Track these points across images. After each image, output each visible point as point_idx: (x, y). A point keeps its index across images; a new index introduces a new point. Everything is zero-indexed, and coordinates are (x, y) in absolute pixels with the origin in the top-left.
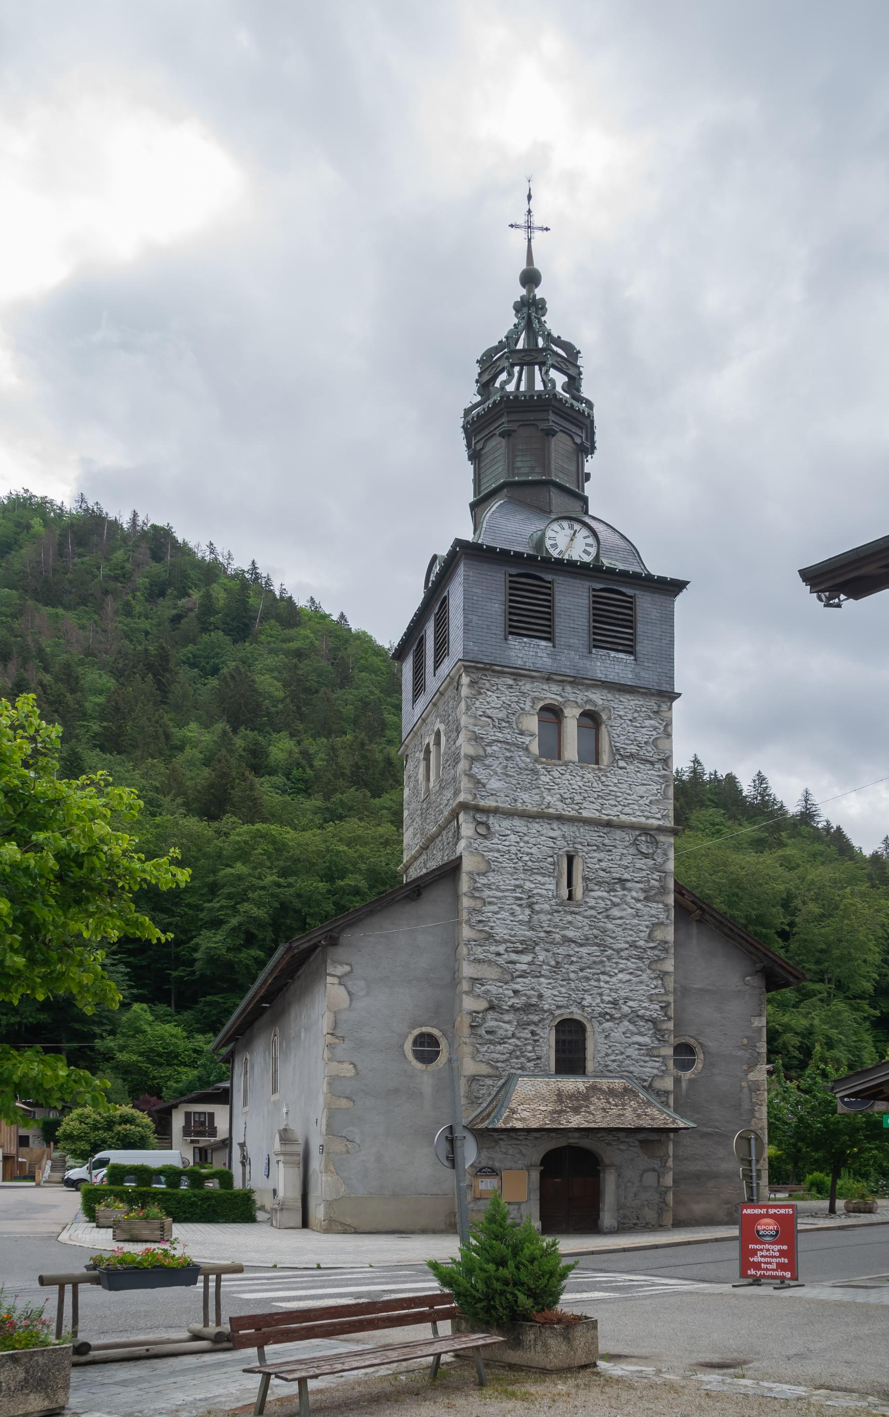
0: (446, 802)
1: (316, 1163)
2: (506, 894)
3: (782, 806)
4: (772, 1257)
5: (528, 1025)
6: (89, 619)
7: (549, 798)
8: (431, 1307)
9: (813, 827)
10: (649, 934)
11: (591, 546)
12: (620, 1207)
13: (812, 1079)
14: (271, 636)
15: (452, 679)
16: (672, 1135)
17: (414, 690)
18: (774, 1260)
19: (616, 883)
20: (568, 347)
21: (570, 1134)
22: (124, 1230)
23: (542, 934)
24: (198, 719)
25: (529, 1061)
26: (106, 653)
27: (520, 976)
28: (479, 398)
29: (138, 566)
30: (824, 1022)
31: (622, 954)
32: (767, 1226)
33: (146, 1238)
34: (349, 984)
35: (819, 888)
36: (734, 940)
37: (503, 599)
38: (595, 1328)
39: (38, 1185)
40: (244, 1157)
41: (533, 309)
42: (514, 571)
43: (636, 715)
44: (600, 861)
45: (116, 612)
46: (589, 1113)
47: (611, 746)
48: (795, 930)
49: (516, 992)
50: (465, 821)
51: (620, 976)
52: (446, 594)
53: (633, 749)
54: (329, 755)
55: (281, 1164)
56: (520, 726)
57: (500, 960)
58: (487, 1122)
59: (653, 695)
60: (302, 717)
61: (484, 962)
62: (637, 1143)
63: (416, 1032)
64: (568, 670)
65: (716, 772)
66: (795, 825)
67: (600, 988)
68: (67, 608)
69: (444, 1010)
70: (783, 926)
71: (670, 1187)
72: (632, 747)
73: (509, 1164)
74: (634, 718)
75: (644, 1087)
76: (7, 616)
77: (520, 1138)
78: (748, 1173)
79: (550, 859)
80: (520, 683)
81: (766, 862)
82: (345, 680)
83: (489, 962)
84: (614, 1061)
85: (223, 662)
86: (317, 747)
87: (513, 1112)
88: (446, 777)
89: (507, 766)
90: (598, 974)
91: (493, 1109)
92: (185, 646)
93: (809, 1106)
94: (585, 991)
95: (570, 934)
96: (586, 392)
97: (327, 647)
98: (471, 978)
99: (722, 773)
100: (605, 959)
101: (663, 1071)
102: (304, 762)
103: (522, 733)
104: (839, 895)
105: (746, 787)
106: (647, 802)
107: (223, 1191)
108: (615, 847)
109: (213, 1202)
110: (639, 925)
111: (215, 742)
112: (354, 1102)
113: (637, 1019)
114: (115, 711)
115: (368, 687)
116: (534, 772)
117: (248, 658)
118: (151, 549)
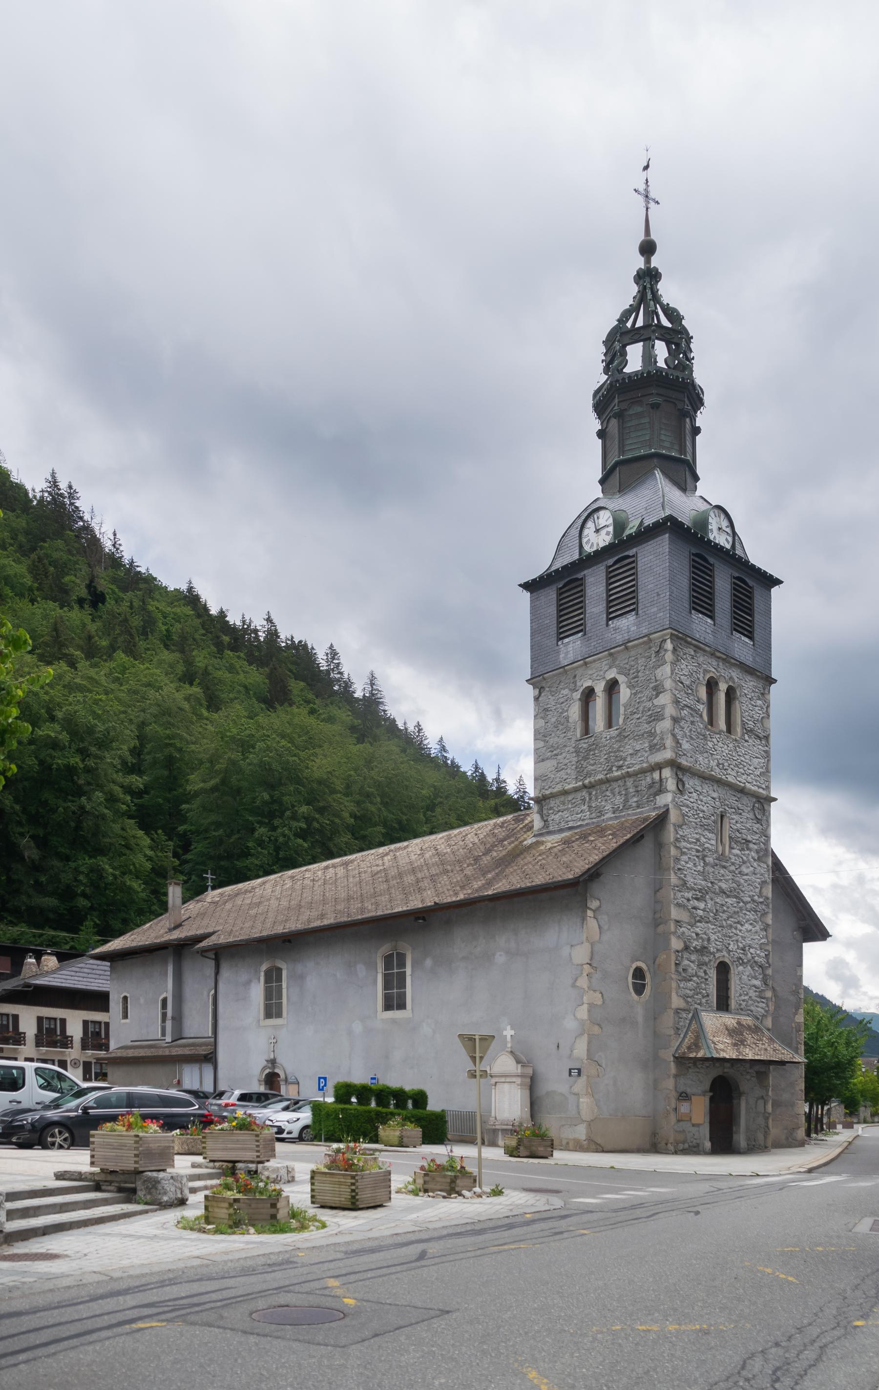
15: (650, 640)
25: (703, 997)
27: (699, 921)
33: (541, 1154)
41: (648, 279)
59: (762, 678)
63: (634, 966)
94: (730, 937)
95: (724, 886)
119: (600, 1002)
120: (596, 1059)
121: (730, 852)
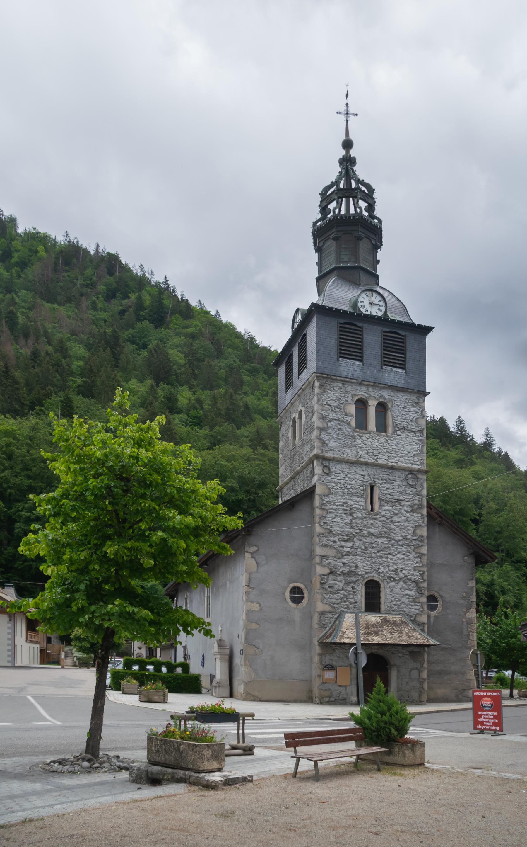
0: (306, 453)
1: (238, 660)
2: (339, 507)
3: (473, 438)
4: (490, 719)
5: (350, 583)
6: (73, 311)
7: (361, 452)
8: (355, 734)
9: (491, 452)
10: (414, 532)
11: (382, 306)
12: (399, 690)
13: (499, 617)
14: (176, 324)
15: (310, 382)
16: (426, 649)
17: (286, 385)
18: (490, 720)
19: (396, 502)
20: (368, 186)
21: (373, 647)
22: (145, 696)
23: (358, 531)
24: (136, 377)
25: (351, 604)
26: (83, 333)
27: (346, 555)
28: (320, 216)
29: (100, 279)
30: (500, 577)
31: (400, 543)
32: (487, 702)
34: (257, 557)
35: (496, 493)
36: (458, 535)
37: (336, 337)
38: (424, 746)
39: (63, 667)
40: (186, 655)
42: (342, 321)
43: (406, 404)
44: (388, 489)
45: (88, 307)
46: (383, 635)
47: (393, 422)
48: (482, 518)
49: (344, 564)
50: (317, 465)
51: (398, 556)
52: (305, 332)
53: (404, 424)
54: (212, 401)
55: (218, 660)
56: (346, 410)
57: (336, 546)
58: (330, 639)
59: (415, 393)
60: (195, 376)
61: (327, 546)
62: (408, 653)
63: (291, 586)
64: (370, 379)
65: (434, 416)
66: (480, 451)
67: (388, 562)
68: (60, 304)
69: (307, 573)
70: (475, 516)
71: (425, 679)
72: (404, 423)
73: (341, 663)
74: (405, 406)
75: (411, 620)
76: (26, 309)
77: (346, 648)
78: (476, 672)
79: (362, 488)
80: (346, 386)
81: (463, 474)
82: (219, 354)
83: (330, 546)
84: (395, 605)
85: (150, 341)
86: (205, 395)
87: (344, 633)
88: (305, 438)
89: (339, 434)
90: (387, 554)
91: (333, 631)
92: (127, 330)
93: (498, 633)
95: (372, 531)
96: (377, 213)
97: (209, 332)
98: (321, 556)
99: (438, 417)
100: (390, 546)
101: (421, 611)
102: (198, 406)
103: (346, 415)
104: (507, 497)
105: (452, 427)
106: (412, 455)
107: (184, 675)
108: (395, 480)
109: (180, 681)
110: (408, 526)
111: (147, 392)
112: (259, 625)
113: (407, 581)
114: (89, 371)
115: (232, 358)
116: (353, 437)
117: (164, 338)
118: (107, 267)
119: (258, 609)
120: (253, 644)
121: (379, 508)
